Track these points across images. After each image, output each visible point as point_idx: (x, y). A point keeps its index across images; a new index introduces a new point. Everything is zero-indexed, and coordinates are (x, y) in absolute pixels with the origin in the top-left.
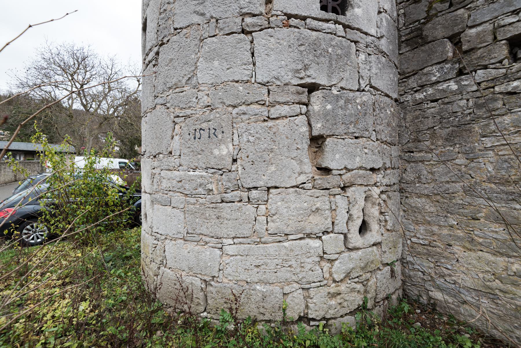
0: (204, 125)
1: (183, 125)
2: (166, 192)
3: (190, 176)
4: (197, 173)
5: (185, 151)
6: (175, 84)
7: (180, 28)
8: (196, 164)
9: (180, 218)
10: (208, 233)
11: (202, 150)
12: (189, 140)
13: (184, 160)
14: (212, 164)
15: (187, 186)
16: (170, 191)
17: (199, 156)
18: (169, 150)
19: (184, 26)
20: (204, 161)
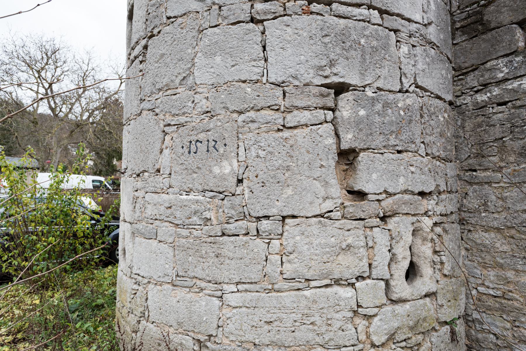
0: (202, 136)
1: (175, 135)
2: (151, 221)
3: (182, 201)
4: (191, 197)
5: (177, 168)
6: (167, 85)
7: (175, 17)
8: (191, 186)
9: (168, 256)
10: (204, 276)
11: (198, 168)
12: (183, 154)
13: (175, 180)
14: (211, 185)
15: (178, 214)
16: (156, 219)
17: (195, 175)
18: (157, 167)
19: (180, 14)
20: (201, 181)
